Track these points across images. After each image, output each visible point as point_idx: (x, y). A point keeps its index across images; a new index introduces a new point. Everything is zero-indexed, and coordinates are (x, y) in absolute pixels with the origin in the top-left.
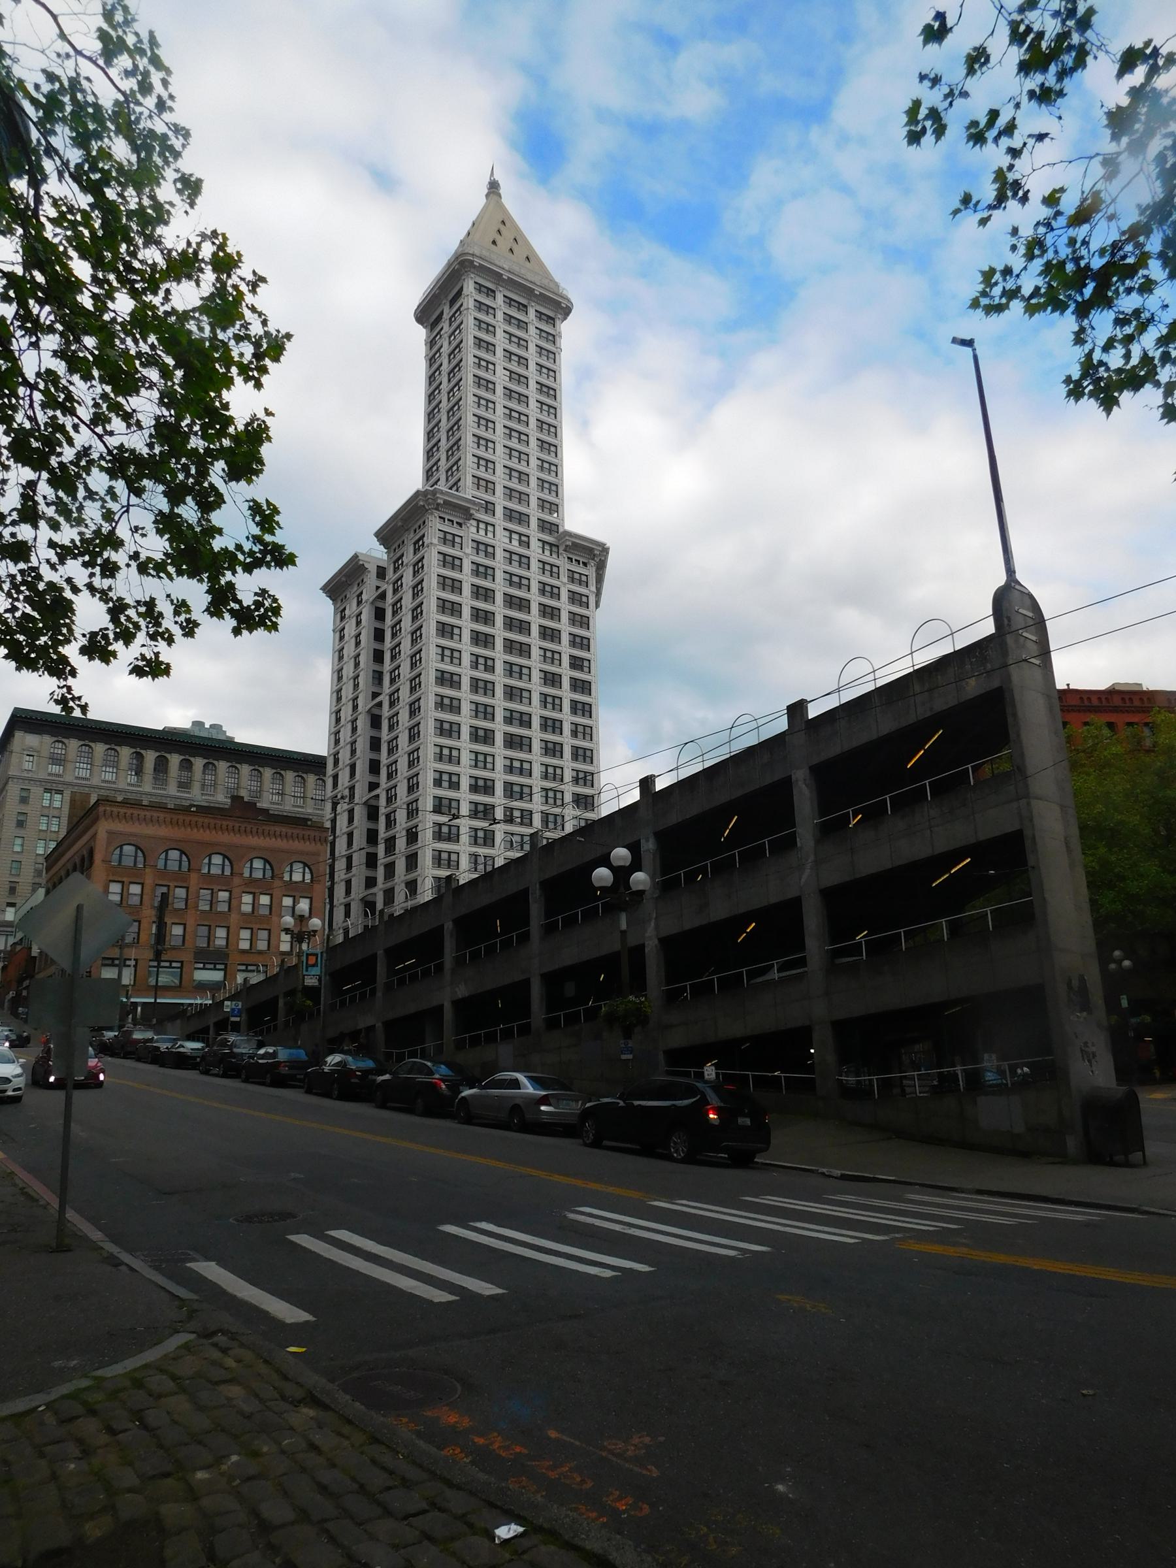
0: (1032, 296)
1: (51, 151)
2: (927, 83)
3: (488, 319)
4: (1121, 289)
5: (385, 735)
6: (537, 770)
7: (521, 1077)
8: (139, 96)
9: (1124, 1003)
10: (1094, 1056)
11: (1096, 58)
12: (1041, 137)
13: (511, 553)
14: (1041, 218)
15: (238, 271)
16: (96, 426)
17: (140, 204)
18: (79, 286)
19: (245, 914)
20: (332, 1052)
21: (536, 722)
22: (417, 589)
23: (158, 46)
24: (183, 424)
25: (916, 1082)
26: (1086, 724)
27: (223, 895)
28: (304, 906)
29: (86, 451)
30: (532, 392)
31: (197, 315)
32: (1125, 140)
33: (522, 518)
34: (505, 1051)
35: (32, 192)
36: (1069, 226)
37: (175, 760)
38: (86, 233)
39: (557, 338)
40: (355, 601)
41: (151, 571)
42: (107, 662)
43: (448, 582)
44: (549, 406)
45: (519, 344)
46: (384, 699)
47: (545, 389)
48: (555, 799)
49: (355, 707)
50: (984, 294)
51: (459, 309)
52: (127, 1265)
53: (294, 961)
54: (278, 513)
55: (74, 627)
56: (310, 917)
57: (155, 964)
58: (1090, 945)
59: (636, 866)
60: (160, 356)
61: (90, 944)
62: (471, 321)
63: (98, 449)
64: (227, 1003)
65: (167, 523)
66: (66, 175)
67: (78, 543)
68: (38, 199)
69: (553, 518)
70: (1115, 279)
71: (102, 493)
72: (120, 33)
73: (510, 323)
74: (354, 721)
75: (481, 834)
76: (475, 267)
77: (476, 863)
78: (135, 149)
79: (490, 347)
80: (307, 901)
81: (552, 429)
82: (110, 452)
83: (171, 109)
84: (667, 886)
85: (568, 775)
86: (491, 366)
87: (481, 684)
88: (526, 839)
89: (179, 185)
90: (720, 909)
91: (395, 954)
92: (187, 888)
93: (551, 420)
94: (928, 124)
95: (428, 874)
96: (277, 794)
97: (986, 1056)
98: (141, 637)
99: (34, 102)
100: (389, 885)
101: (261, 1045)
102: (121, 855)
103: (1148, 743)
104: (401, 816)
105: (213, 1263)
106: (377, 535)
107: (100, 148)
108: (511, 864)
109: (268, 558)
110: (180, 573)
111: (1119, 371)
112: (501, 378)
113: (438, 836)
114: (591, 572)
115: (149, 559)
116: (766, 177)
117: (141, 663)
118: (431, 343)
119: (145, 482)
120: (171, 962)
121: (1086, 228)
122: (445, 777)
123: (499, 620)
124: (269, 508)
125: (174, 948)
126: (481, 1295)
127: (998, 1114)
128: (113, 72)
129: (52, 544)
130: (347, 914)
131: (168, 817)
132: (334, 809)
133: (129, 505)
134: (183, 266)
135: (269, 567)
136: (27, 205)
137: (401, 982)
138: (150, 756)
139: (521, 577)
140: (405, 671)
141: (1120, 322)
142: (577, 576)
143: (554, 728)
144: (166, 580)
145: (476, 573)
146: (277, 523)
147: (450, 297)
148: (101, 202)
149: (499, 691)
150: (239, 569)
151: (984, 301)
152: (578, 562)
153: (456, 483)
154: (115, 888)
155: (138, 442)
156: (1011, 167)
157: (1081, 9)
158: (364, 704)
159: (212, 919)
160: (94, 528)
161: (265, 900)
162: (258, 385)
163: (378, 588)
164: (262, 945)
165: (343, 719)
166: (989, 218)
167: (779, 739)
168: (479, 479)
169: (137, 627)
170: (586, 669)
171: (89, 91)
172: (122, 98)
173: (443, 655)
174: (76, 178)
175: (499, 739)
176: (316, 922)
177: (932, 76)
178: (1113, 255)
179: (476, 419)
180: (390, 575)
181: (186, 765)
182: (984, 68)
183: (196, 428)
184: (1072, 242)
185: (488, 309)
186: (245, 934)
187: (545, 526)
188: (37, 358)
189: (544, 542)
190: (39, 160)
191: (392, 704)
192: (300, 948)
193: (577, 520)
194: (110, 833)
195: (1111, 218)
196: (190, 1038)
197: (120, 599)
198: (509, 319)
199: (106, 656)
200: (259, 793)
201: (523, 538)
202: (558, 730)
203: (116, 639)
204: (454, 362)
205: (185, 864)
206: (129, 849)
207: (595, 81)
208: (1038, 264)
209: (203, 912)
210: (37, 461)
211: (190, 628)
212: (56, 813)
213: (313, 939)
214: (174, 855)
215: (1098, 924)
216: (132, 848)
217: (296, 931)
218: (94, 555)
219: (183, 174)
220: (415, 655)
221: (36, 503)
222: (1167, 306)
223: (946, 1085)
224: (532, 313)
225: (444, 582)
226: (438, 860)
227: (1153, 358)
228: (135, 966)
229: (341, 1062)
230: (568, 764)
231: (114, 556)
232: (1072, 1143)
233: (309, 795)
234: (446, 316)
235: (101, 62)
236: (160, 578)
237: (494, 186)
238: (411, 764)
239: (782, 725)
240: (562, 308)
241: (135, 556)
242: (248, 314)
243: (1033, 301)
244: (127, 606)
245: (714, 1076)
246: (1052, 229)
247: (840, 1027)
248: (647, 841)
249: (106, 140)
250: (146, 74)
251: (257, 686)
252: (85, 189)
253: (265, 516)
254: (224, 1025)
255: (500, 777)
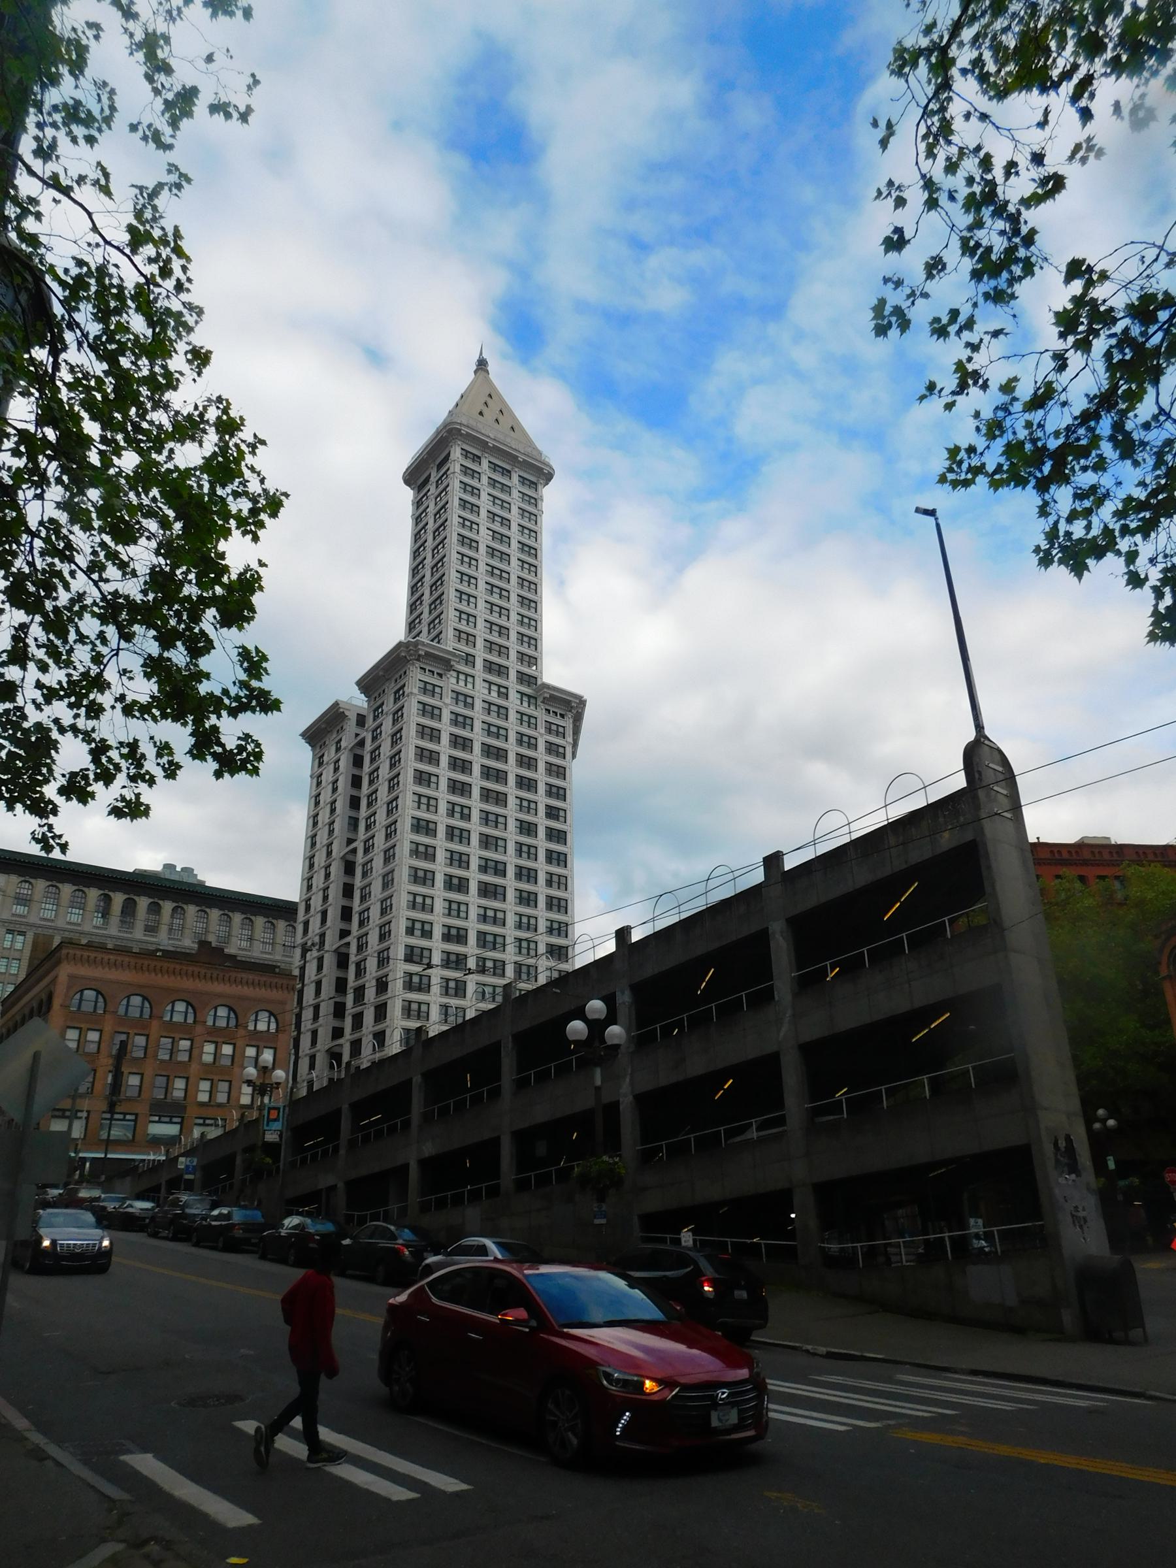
0: (995, 472)
1: (73, 325)
2: (890, 285)
3: (474, 483)
4: (1077, 468)
5: (358, 882)
6: (511, 920)
7: (488, 1243)
8: (159, 280)
9: (1111, 1165)
10: (1085, 1221)
11: (1042, 268)
12: (996, 334)
13: (490, 704)
14: (999, 403)
15: (240, 434)
16: (94, 572)
17: (151, 371)
18: (87, 441)
19: (206, 1065)
20: (289, 1214)
21: (511, 871)
22: (396, 737)
23: (181, 238)
24: (178, 572)
25: (903, 1250)
26: (1058, 877)
27: (185, 1044)
28: (267, 1056)
29: (81, 596)
30: (514, 550)
31: (198, 473)
32: (1071, 339)
33: (501, 671)
34: (472, 1214)
35: (51, 359)
36: (1024, 411)
37: (143, 903)
38: (99, 397)
39: (539, 502)
40: (333, 748)
41: (137, 714)
42: (85, 803)
43: (427, 731)
44: (530, 565)
45: (502, 507)
46: (359, 845)
47: (526, 549)
48: (528, 949)
49: (329, 853)
50: (950, 470)
51: (445, 473)
52: (54, 1460)
53: (255, 1115)
54: (267, 660)
55: (54, 767)
56: (274, 1068)
57: (108, 1116)
58: (1075, 1104)
59: (611, 1019)
60: (160, 508)
61: (45, 1093)
62: (457, 484)
63: (93, 594)
64: (182, 1159)
65: (155, 667)
66: (85, 345)
67: (65, 685)
68: (56, 366)
69: (532, 671)
70: (1070, 458)
71: (93, 637)
72: (148, 227)
73: (494, 487)
74: (328, 867)
75: (452, 984)
76: (462, 435)
77: (446, 1014)
78: (151, 324)
79: (474, 508)
80: (271, 1051)
81: (533, 586)
82: (104, 598)
83: (188, 290)
84: (642, 1041)
85: (542, 926)
86: (475, 526)
87: (457, 832)
88: (498, 990)
89: (189, 356)
90: (697, 1065)
91: (361, 1109)
92: (148, 1036)
93: (531, 578)
94: (893, 319)
95: (398, 1025)
96: (245, 940)
97: (972, 1221)
98: (121, 779)
99: (62, 283)
100: (356, 1036)
101: (213, 1208)
102: (81, 1000)
103: (1119, 896)
104: (371, 964)
105: (149, 1456)
106: (358, 683)
107: (118, 323)
108: (483, 1016)
109: (254, 703)
110: (164, 716)
111: (1081, 541)
112: (484, 538)
113: (409, 986)
114: (568, 723)
115: (135, 702)
116: (730, 363)
117: (120, 804)
118: (418, 503)
119: (136, 628)
120: (125, 1114)
121: (1041, 412)
122: (418, 926)
123: (476, 770)
124: (257, 655)
125: (129, 1099)
126: (444, 1492)
127: (990, 1284)
128: (137, 259)
129: (39, 685)
130: (312, 1066)
131: (133, 961)
132: (303, 956)
133: (118, 649)
134: (188, 428)
135: (254, 712)
136: (46, 371)
137: (366, 1139)
138: (118, 899)
139: (499, 728)
140: (381, 818)
141: (1079, 496)
142: (554, 727)
143: (529, 876)
144: (150, 723)
145: (455, 723)
146: (265, 670)
147: (437, 462)
148: (115, 369)
149: (475, 839)
150: (224, 713)
151: (950, 476)
152: (556, 713)
153: (438, 636)
154: (72, 1034)
155: (133, 589)
156: (970, 359)
157: (1024, 230)
158: (338, 850)
159: (171, 1069)
160: (82, 670)
161: (227, 1050)
162: (256, 539)
163: (357, 735)
164: (222, 1098)
165: (316, 865)
166: (953, 404)
167: (755, 891)
168: (460, 632)
169: (118, 768)
170: (562, 819)
171: (115, 275)
172: (142, 280)
173: (419, 803)
174: (93, 348)
175: (473, 887)
176: (279, 1074)
177: (895, 279)
178: (1067, 437)
179: (459, 575)
180: (370, 723)
181: (155, 909)
182: (942, 274)
183: (192, 576)
184: (1029, 425)
185: (474, 474)
186: (205, 1085)
187: (523, 678)
188: (40, 508)
189: (522, 694)
190: (61, 331)
191: (366, 851)
192: (262, 1101)
193: (555, 673)
194: (71, 977)
195: (1064, 404)
196: (140, 1197)
197: (103, 740)
198: (493, 483)
199: (84, 797)
200: (227, 939)
201: (502, 690)
202: (532, 880)
203: (96, 780)
204: (440, 522)
205: (147, 1011)
206: (89, 994)
207: (570, 277)
208: (999, 445)
209: (162, 1061)
210: (32, 606)
211: (172, 771)
212: (17, 955)
213: (275, 1091)
214: (136, 1000)
215: (1081, 1081)
216: (93, 993)
217: (258, 1083)
218: (80, 697)
219: (194, 347)
220: (391, 802)
221: (26, 646)
222: (1120, 483)
223: (931, 1254)
224: (515, 478)
225: (423, 731)
226: (407, 1011)
227: (1113, 530)
228: (87, 1118)
229: (299, 1225)
230: (542, 914)
231: (100, 699)
232: (1068, 1318)
233: (278, 940)
234: (433, 479)
235: (127, 251)
236: (145, 719)
237: (482, 364)
238: (384, 912)
239: (758, 876)
240: (544, 474)
241: (122, 698)
242: (247, 474)
243: (997, 477)
244: (110, 747)
245: (691, 1243)
246: (1010, 414)
247: (825, 1191)
248: (623, 993)
249: (125, 315)
250: (168, 260)
251: (230, 832)
252: (100, 358)
253: (253, 662)
254: (177, 1183)
255: (473, 926)
